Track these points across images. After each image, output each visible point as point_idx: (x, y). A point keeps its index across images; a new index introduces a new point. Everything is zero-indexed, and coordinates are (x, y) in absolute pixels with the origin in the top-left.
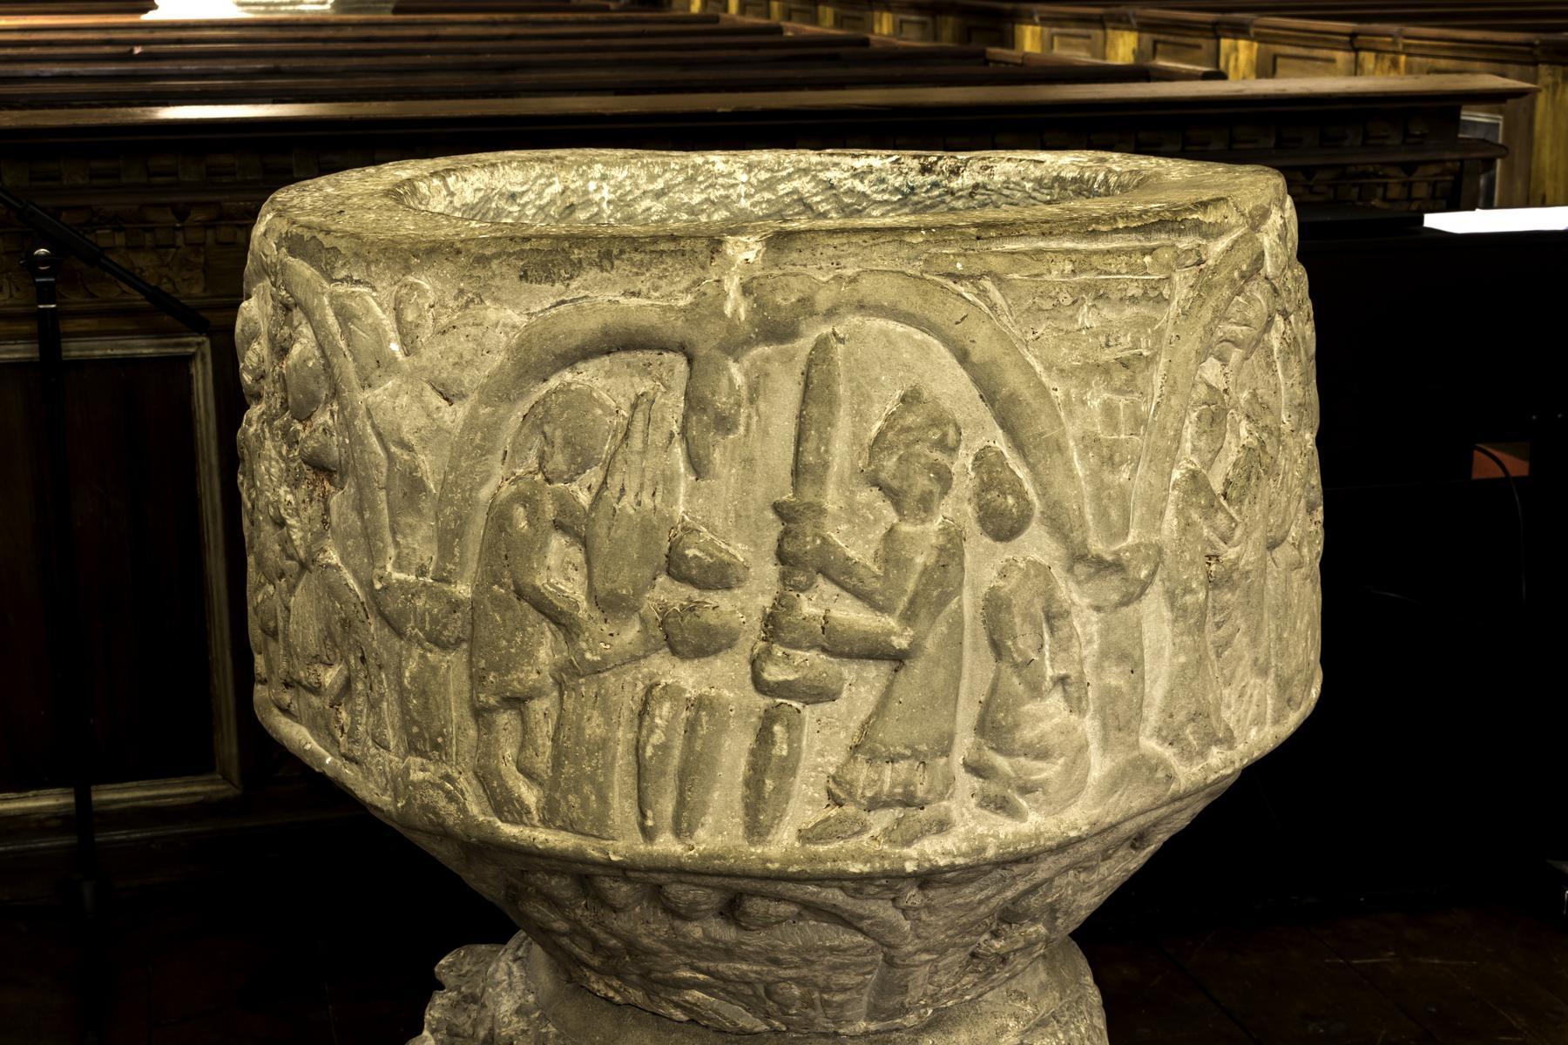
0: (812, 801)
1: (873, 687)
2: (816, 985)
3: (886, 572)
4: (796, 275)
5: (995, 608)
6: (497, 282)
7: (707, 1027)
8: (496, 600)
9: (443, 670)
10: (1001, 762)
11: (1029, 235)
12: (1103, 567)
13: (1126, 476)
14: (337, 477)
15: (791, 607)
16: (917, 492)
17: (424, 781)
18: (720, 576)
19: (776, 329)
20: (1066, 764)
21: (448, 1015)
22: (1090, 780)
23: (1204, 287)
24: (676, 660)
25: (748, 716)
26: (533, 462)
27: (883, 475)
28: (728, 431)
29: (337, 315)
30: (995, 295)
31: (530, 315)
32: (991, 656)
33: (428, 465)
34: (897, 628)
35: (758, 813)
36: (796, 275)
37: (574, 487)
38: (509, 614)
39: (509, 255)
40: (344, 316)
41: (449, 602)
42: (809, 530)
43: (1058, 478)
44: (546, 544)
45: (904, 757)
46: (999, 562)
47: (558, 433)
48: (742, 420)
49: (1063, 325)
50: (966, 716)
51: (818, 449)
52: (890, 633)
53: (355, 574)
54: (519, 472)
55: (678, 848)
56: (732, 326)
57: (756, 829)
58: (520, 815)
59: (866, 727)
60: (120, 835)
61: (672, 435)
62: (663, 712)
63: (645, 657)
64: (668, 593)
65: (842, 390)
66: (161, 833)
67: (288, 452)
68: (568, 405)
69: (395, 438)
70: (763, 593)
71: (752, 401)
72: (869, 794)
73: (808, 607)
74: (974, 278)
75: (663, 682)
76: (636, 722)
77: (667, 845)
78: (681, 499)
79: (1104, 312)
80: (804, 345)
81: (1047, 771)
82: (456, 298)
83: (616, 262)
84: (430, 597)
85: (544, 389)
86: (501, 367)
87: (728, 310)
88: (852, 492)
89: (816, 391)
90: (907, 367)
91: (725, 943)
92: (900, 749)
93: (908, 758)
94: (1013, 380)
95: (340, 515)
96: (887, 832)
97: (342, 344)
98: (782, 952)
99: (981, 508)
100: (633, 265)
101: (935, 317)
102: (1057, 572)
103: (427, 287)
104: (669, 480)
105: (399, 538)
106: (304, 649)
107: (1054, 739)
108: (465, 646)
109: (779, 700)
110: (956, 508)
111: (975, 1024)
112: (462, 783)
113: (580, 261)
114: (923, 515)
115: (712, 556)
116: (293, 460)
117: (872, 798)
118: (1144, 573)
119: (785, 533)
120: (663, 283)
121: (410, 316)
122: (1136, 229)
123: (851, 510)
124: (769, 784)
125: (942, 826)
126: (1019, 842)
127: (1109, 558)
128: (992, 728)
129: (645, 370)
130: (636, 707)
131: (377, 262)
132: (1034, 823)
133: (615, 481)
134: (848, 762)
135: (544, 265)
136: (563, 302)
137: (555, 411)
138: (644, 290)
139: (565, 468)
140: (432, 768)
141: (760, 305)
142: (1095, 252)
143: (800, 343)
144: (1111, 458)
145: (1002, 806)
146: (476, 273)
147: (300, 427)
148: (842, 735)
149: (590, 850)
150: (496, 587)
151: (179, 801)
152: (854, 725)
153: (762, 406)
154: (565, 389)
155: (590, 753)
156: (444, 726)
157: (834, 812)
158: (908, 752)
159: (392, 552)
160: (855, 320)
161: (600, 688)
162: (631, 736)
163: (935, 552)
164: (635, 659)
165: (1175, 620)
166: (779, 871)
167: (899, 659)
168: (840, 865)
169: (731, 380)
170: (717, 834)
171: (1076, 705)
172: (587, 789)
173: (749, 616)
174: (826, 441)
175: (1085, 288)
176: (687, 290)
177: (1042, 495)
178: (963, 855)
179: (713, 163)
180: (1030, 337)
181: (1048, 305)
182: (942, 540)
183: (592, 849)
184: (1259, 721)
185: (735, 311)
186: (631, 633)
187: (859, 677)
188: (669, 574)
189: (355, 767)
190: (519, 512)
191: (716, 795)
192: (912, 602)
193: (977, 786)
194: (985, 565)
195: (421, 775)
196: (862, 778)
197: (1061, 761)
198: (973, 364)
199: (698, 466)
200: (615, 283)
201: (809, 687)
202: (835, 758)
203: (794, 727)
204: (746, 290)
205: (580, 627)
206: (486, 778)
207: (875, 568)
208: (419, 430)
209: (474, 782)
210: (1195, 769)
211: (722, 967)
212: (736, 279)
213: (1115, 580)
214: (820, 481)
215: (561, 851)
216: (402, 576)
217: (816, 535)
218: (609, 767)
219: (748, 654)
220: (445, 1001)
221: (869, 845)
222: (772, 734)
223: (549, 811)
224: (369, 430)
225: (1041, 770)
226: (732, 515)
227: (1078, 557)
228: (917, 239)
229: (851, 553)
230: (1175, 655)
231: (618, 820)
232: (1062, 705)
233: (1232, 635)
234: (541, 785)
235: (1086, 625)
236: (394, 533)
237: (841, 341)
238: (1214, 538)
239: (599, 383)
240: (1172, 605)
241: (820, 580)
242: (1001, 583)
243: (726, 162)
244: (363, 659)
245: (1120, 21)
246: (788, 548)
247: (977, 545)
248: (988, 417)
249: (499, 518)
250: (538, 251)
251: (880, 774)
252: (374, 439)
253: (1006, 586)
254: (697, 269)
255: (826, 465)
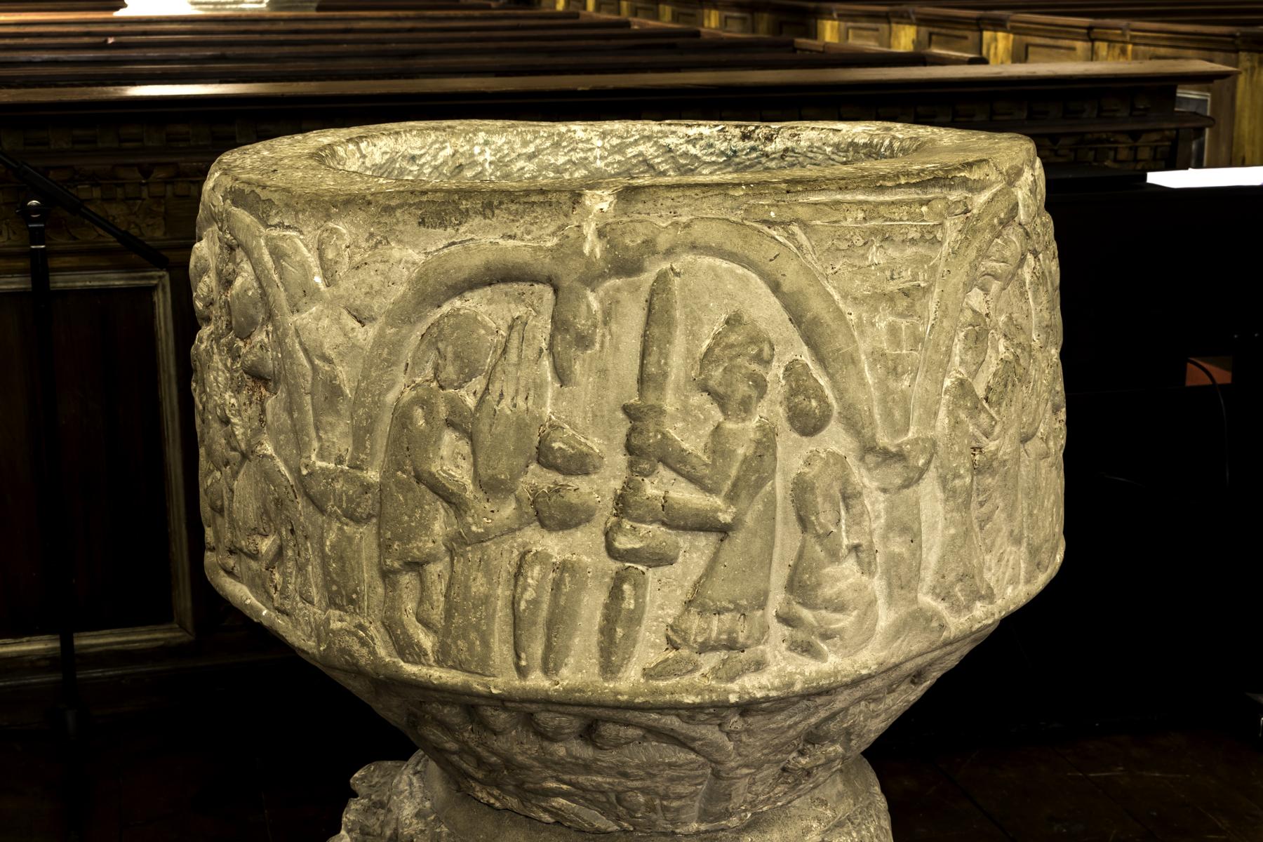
0: (654, 646)
1: (703, 553)
2: (657, 794)
3: (714, 461)
4: (641, 222)
5: (801, 490)
6: (401, 227)
7: (569, 827)
8: (399, 483)
9: (357, 540)
10: (807, 614)
11: (829, 190)
12: (888, 457)
13: (907, 383)
14: (271, 384)
15: (637, 489)
16: (738, 396)
17: (341, 629)
18: (580, 464)
19: (625, 265)
20: (859, 616)
21: (361, 818)
22: (878, 628)
23: (970, 231)
24: (545, 532)
25: (603, 577)
26: (429, 372)
27: (711, 383)
28: (587, 347)
29: (271, 253)
30: (802, 237)
31: (427, 254)
32: (798, 529)
33: (345, 375)
34: (723, 506)
35: (610, 655)
36: (641, 222)
37: (463, 392)
38: (410, 495)
39: (410, 205)
40: (277, 254)
41: (362, 485)
42: (652, 427)
43: (852, 385)
44: (439, 438)
45: (728, 610)
46: (805, 453)
47: (450, 349)
48: (598, 338)
49: (856, 262)
50: (778, 577)
51: (659, 362)
52: (717, 510)
53: (286, 462)
54: (418, 380)
55: (546, 684)
56: (589, 262)
57: (609, 668)
58: (419, 657)
59: (698, 586)
60: (97, 673)
61: (541, 350)
62: (534, 574)
63: (519, 529)
64: (538, 478)
65: (678, 314)
66: (130, 671)
67: (232, 364)
68: (458, 327)
69: (318, 353)
70: (615, 478)
71: (605, 323)
72: (700, 640)
73: (651, 489)
74: (784, 224)
75: (534, 550)
76: (513, 581)
77: (537, 681)
78: (549, 402)
79: (889, 251)
80: (647, 278)
81: (844, 621)
82: (367, 240)
83: (497, 211)
84: (346, 481)
85: (438, 313)
86: (404, 296)
87: (586, 250)
88: (686, 397)
89: (657, 315)
90: (730, 295)
91: (584, 760)
92: (725, 604)
93: (732, 610)
94: (816, 306)
95: (274, 415)
96: (714, 670)
97: (276, 277)
98: (630, 767)
99: (790, 409)
100: (510, 213)
101: (753, 256)
102: (852, 461)
103: (344, 231)
104: (539, 387)
105: (321, 434)
106: (245, 523)
107: (849, 596)
108: (374, 520)
109: (627, 564)
110: (770, 409)
111: (786, 825)
112: (372, 631)
113: (467, 210)
114: (743, 415)
115: (573, 448)
116: (236, 371)
117: (703, 643)
118: (921, 462)
119: (633, 429)
120: (534, 228)
121: (330, 254)
122: (915, 185)
123: (686, 411)
124: (620, 632)
125: (759, 665)
126: (821, 678)
127: (894, 450)
128: (799, 586)
129: (520, 298)
130: (512, 570)
131: (304, 211)
132: (833, 663)
133: (496, 388)
134: (683, 614)
135: (438, 214)
136: (454, 243)
137: (447, 331)
138: (519, 234)
139: (455, 377)
140: (348, 618)
141: (612, 246)
142: (882, 203)
143: (644, 276)
144: (895, 369)
145: (807, 649)
146: (383, 220)
147: (241, 344)
148: (679, 592)
149: (475, 685)
150: (399, 473)
151: (144, 645)
152: (688, 584)
153: (614, 327)
154: (455, 314)
155: (475, 607)
156: (358, 585)
157: (672, 654)
158: (731, 606)
159: (316, 444)
160: (689, 258)
161: (483, 554)
162: (508, 593)
163: (753, 445)
164: (512, 531)
165: (947, 500)
166: (627, 702)
167: (724, 531)
168: (677, 697)
169: (589, 306)
170: (578, 672)
171: (867, 568)
172: (473, 635)
173: (603, 496)
174: (665, 355)
175: (874, 232)
176: (554, 234)
177: (840, 399)
178: (776, 689)
179: (575, 132)
180: (830, 271)
181: (844, 245)
182: (758, 435)
183: (477, 684)
184: (1014, 581)
185: (592, 251)
186: (508, 510)
187: (692, 545)
188: (539, 462)
189: (286, 618)
190: (418, 413)
191: (577, 640)
192: (735, 485)
193: (787, 633)
194: (793, 455)
195: (339, 624)
196: (694, 627)
197: (855, 613)
198: (784, 294)
199: (562, 375)
200: (495, 228)
201: (652, 554)
202: (673, 611)
203: (639, 586)
204: (601, 233)
205: (467, 505)
206: (392, 627)
207: (705, 458)
208: (337, 346)
209: (382, 630)
210: (963, 620)
211: (581, 779)
212: (593, 225)
213: (898, 467)
214: (661, 387)
215: (452, 686)
216: (324, 464)
217: (657, 431)
218: (490, 618)
219: (602, 527)
220: (359, 807)
221: (700, 681)
222: (622, 591)
223: (443, 654)
224: (297, 346)
225: (838, 621)
226: (590, 415)
227: (868, 449)
228: (739, 192)
229: (685, 445)
230: (946, 528)
231: (498, 661)
232: (856, 568)
233: (993, 512)
234: (435, 632)
235: (875, 504)
236: (317, 429)
237: (678, 274)
238: (978, 433)
239: (482, 309)
240: (944, 487)
241: (661, 467)
242: (807, 470)
243: (585, 131)
244: (292, 531)
245: (902, 17)
246: (634, 442)
247: (787, 439)
248: (796, 336)
249: (402, 417)
250: (433, 202)
251: (709, 623)
252: (301, 354)
253: (811, 472)
254: (562, 217)
255: (665, 375)
